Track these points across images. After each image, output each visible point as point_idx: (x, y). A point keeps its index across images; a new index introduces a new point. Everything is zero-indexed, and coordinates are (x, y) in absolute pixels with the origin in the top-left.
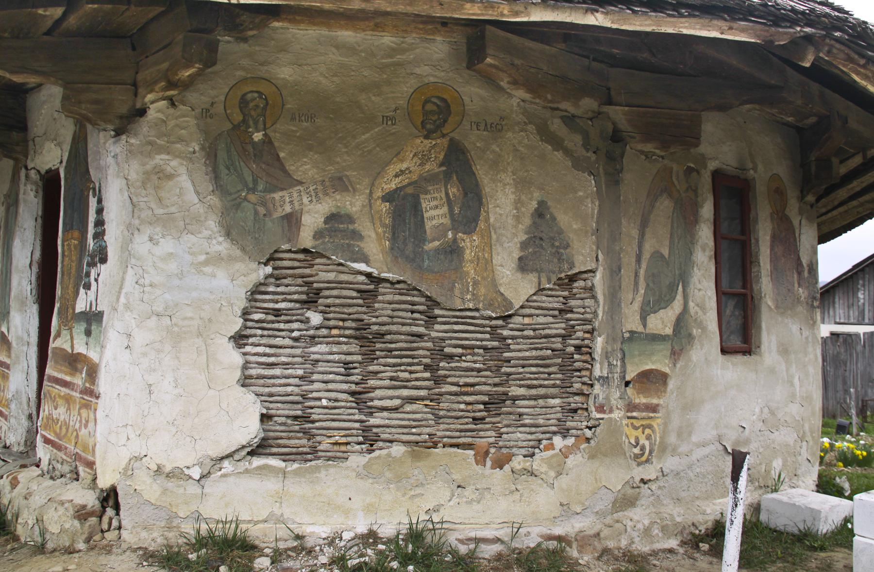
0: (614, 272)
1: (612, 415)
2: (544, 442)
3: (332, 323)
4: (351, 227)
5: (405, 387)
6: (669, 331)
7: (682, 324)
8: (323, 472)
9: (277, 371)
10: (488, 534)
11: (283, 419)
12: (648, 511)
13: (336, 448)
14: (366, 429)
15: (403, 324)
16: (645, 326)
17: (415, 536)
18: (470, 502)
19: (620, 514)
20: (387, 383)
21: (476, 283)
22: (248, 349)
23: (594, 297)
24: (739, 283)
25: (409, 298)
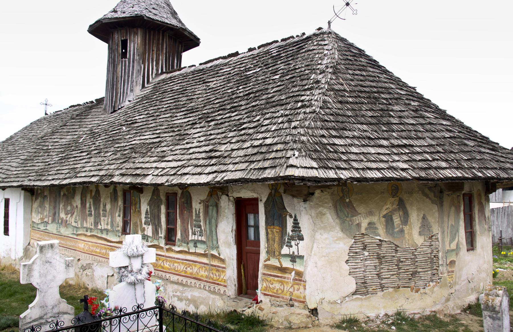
0: (443, 233)
2: (428, 284)
3: (371, 254)
4: (375, 226)
5: (391, 271)
6: (455, 248)
8: (372, 298)
9: (358, 270)
10: (416, 312)
11: (360, 284)
13: (373, 290)
14: (381, 284)
15: (390, 253)
17: (398, 314)
18: (410, 303)
20: (386, 270)
21: (408, 240)
22: (349, 264)
23: (438, 241)
24: (470, 227)
25: (391, 246)
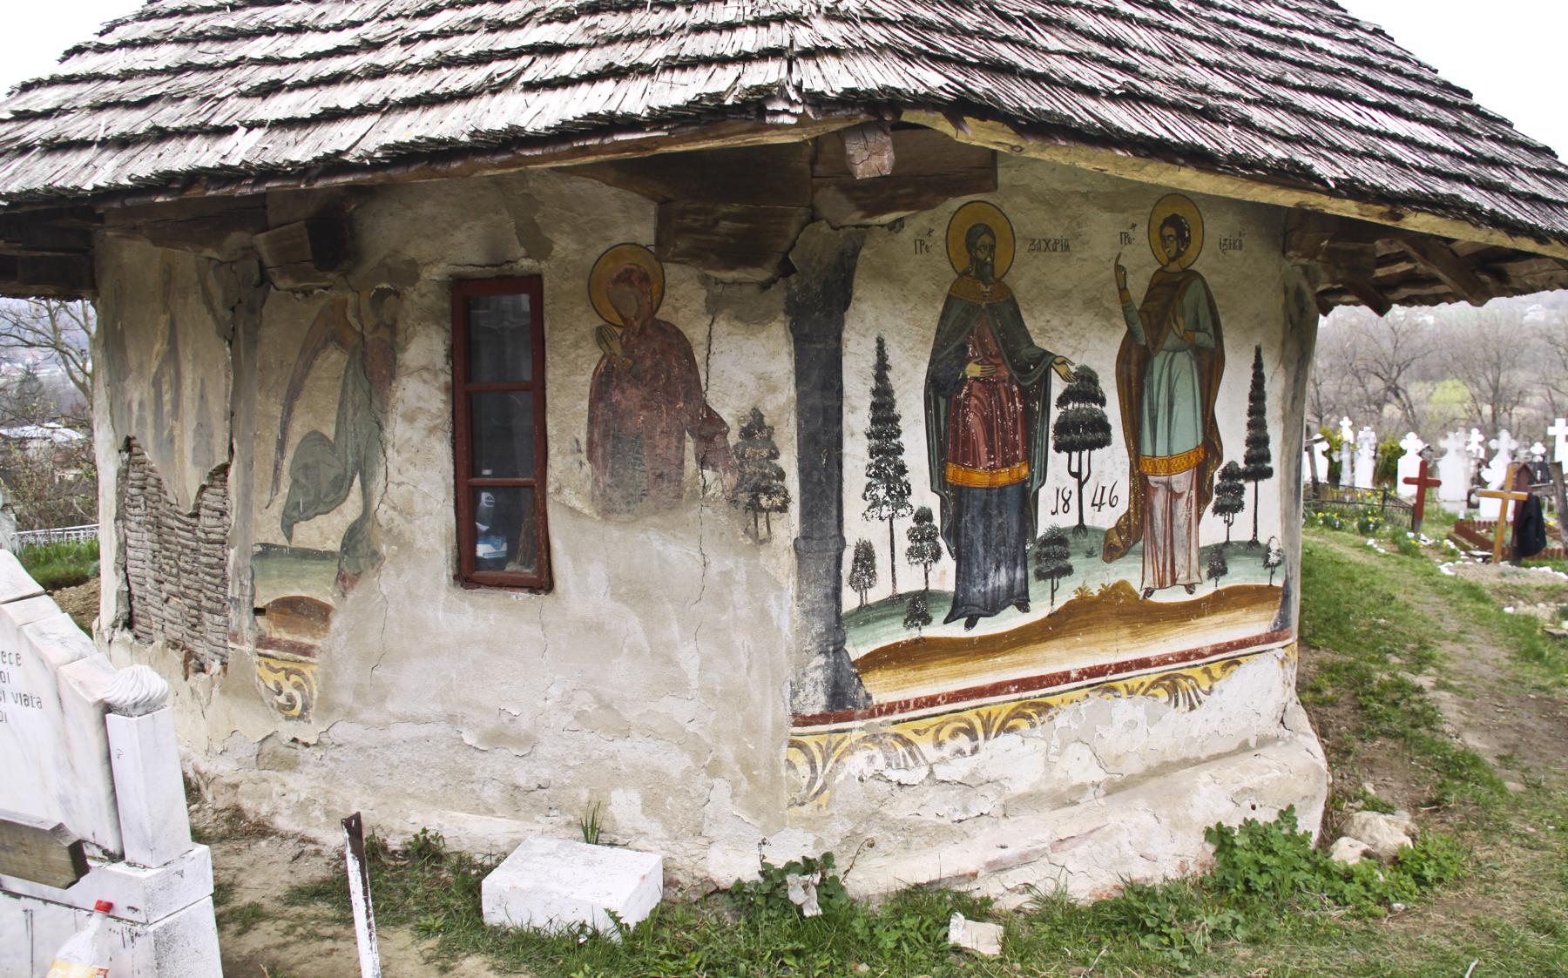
1: (243, 648)
6: (334, 545)
7: (359, 537)
12: (314, 783)
16: (289, 538)
19: (271, 773)
